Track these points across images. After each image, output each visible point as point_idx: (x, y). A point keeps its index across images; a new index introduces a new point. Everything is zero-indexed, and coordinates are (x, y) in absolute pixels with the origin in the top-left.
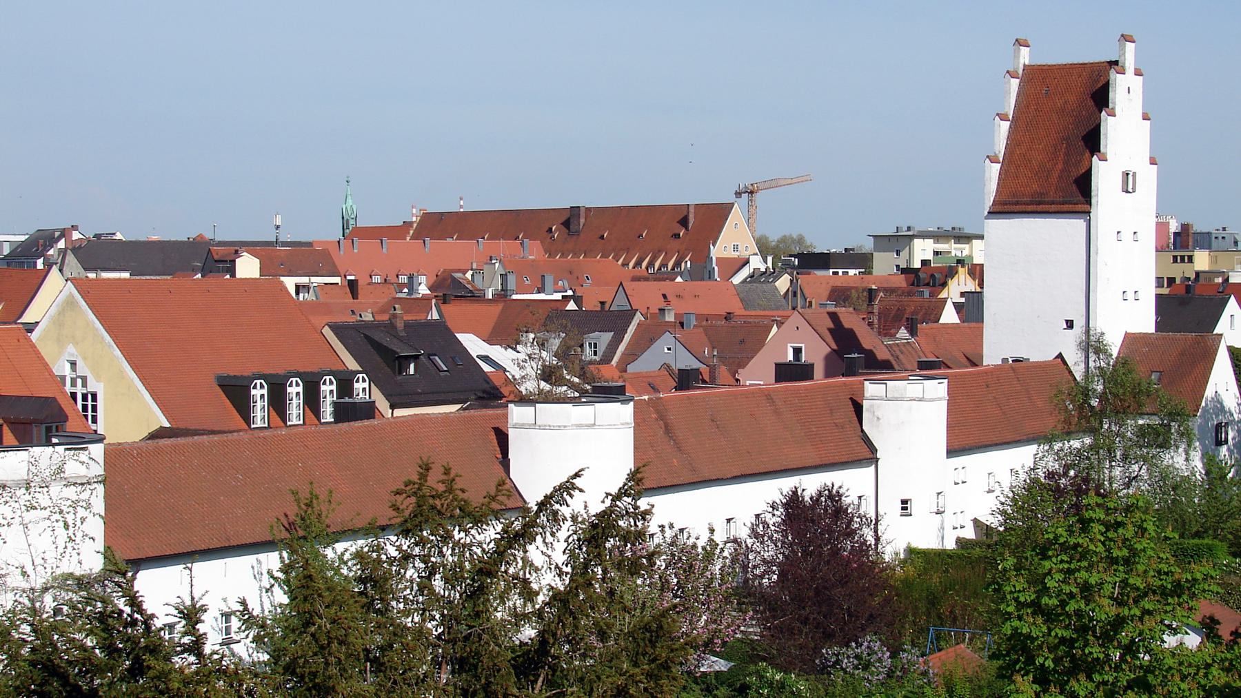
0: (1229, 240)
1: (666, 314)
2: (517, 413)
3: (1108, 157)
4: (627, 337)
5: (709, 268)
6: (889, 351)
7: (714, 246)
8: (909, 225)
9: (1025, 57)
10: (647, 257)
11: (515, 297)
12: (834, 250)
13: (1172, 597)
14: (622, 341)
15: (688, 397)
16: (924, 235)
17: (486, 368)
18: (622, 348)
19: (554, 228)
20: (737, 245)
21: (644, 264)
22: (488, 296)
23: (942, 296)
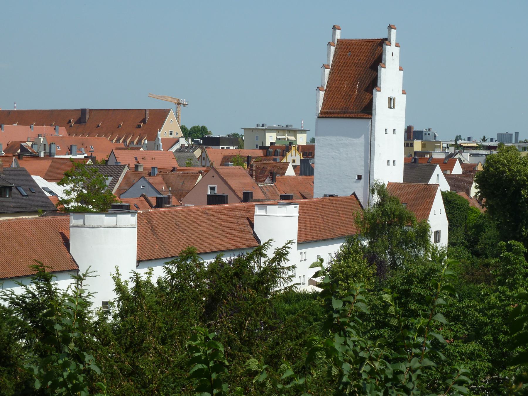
0: (432, 136)
1: (139, 168)
2: (74, 220)
3: (381, 89)
4: (120, 180)
5: (157, 144)
6: (261, 189)
7: (160, 131)
8: (263, 123)
9: (338, 35)
10: (123, 137)
11: (56, 157)
12: (222, 136)
13: (149, 378)
14: (117, 182)
15: (164, 212)
16: (271, 130)
17: (48, 195)
18: (117, 185)
19: (72, 120)
20: (172, 132)
21: (121, 141)
22: (41, 155)
23: (284, 161)
